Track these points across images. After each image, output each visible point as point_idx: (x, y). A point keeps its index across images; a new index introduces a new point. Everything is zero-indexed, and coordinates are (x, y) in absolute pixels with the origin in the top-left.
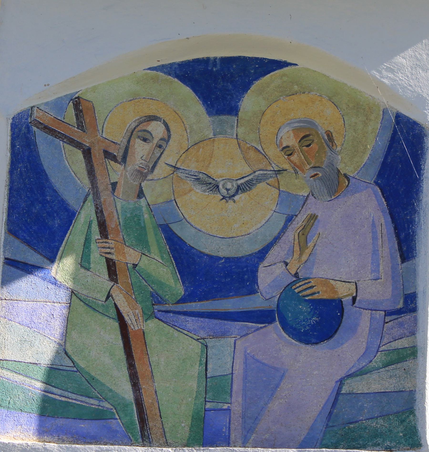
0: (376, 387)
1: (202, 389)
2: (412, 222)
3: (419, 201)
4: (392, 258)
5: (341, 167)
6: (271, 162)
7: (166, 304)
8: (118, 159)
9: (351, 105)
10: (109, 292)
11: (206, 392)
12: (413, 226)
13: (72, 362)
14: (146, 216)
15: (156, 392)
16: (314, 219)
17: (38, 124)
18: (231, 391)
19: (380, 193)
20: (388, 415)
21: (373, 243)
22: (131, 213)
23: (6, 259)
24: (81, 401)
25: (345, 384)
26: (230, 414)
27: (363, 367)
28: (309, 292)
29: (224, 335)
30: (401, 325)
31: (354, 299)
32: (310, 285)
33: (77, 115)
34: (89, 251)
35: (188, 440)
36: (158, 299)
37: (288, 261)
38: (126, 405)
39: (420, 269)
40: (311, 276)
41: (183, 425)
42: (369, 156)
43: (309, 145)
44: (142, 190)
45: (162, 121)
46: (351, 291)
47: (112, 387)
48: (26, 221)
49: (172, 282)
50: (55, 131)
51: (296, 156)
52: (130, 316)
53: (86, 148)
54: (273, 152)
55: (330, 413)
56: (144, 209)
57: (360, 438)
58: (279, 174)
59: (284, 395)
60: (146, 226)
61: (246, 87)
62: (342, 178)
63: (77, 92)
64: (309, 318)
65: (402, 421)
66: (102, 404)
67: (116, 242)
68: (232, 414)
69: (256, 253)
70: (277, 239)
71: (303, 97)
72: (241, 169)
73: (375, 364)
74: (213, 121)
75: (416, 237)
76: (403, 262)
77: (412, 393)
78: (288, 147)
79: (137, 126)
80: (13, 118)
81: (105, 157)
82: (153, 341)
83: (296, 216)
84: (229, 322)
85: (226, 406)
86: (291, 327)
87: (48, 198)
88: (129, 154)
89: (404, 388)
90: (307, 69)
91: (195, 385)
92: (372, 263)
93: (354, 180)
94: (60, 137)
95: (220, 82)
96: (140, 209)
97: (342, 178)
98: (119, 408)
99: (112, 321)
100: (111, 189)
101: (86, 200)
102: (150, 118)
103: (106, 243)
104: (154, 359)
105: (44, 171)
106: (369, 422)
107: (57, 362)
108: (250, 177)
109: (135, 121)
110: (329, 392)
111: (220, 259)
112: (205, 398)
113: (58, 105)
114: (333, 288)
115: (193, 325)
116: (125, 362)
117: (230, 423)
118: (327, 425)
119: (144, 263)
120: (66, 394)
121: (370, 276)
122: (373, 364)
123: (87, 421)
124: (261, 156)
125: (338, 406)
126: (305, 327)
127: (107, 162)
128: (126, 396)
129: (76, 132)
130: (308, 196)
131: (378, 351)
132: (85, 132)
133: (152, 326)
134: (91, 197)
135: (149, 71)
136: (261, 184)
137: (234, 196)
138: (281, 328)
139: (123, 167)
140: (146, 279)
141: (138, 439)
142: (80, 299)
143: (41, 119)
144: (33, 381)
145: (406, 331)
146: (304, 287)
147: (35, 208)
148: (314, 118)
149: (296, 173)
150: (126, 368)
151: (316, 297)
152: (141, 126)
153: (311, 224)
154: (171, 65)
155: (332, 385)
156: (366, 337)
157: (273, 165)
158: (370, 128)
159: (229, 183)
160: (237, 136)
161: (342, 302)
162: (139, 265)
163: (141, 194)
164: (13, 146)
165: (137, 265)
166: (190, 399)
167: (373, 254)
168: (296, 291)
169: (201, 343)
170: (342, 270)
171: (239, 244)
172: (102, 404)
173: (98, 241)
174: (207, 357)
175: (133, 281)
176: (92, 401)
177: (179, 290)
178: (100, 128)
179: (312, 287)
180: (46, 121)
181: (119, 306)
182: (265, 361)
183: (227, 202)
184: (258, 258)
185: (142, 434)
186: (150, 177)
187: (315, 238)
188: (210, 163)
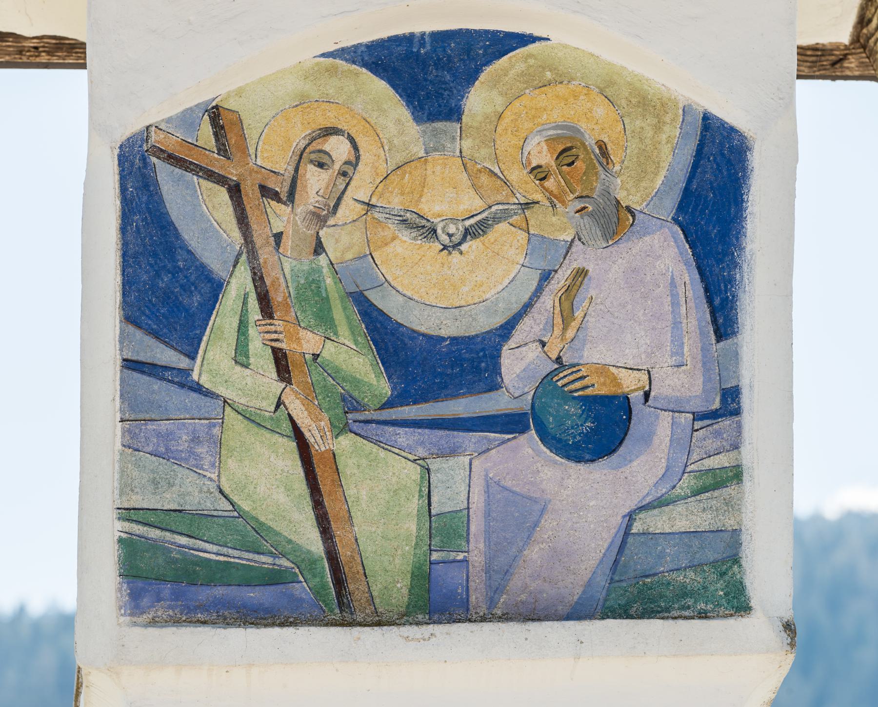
0: (682, 525)
1: (425, 532)
2: (730, 281)
3: (742, 249)
4: (703, 334)
5: (621, 195)
6: (515, 191)
7: (365, 410)
8: (282, 197)
9: (634, 101)
10: (280, 398)
11: (430, 537)
12: (732, 286)
13: (231, 504)
14: (329, 281)
15: (356, 540)
16: (583, 275)
17: (159, 152)
18: (468, 534)
19: (682, 236)
20: (701, 565)
21: (673, 312)
22: (307, 278)
23: (124, 360)
24: (248, 560)
25: (637, 520)
26: (468, 567)
27: (663, 495)
28: (578, 385)
29: (453, 452)
30: (718, 434)
31: (647, 395)
32: (580, 374)
33: (216, 134)
34: (247, 338)
35: (408, 607)
36: (352, 404)
37: (545, 339)
38: (313, 562)
39: (748, 498)
40: (581, 362)
41: (399, 585)
42: (663, 178)
43: (573, 163)
44: (321, 242)
45: (346, 135)
46: (641, 383)
47: (292, 537)
48: (150, 301)
49: (372, 378)
50: (185, 161)
51: (552, 180)
52: (313, 432)
53: (232, 184)
54: (517, 175)
55: (616, 562)
56: (325, 271)
57: (661, 598)
58: (528, 208)
59: (546, 537)
60: (330, 296)
61: (472, 77)
62: (624, 213)
63: (214, 99)
64: (579, 423)
65: (723, 574)
66: (277, 561)
67: (285, 323)
68: (470, 567)
69: (496, 329)
70: (527, 307)
71: (561, 89)
72: (470, 203)
73: (679, 491)
74: (424, 131)
75: (738, 303)
76: (718, 340)
77: (736, 533)
78: (539, 167)
79: (309, 144)
80: (121, 147)
81: (263, 196)
82: (348, 465)
83: (556, 271)
84: (461, 434)
85: (461, 556)
86: (554, 438)
87: (181, 264)
88: (298, 188)
89: (724, 525)
90: (565, 46)
91: (414, 528)
92: (672, 341)
93: (642, 215)
94: (192, 170)
95: (431, 73)
96: (319, 270)
97: (624, 213)
98: (303, 566)
99: (285, 440)
100: (273, 243)
101: (237, 263)
102: (326, 131)
103: (271, 324)
104: (350, 492)
105: (172, 224)
106: (674, 575)
107: (209, 505)
108: (484, 215)
109: (304, 138)
110: (614, 531)
111: (443, 339)
112: (430, 545)
113: (186, 119)
114: (615, 378)
115: (408, 439)
116: (308, 499)
117: (467, 581)
118: (612, 579)
119: (329, 352)
120: (225, 550)
121: (672, 361)
122: (678, 491)
123: (257, 588)
124: (499, 182)
125: (627, 551)
126: (575, 437)
127: (266, 203)
128: (313, 549)
129: (217, 160)
130: (572, 241)
131: (684, 473)
132: (229, 158)
133: (345, 443)
134: (244, 257)
135: (322, 59)
136: (500, 225)
137: (460, 244)
138: (538, 439)
139: (290, 209)
140: (333, 375)
141: (334, 609)
142: (236, 411)
143: (162, 143)
144: (175, 536)
145: (725, 444)
146: (571, 378)
147: (162, 280)
148: (578, 121)
149: (554, 206)
150: (311, 507)
151: (589, 392)
152: (314, 144)
153: (578, 283)
154: (356, 47)
155: (617, 520)
156: (666, 451)
157: (518, 195)
158: (664, 137)
159: (451, 226)
160: (461, 152)
161: (628, 399)
162: (323, 355)
163: (319, 248)
164: (123, 189)
165: (318, 355)
166: (407, 548)
167: (673, 328)
168: (560, 384)
169: (419, 465)
170: (627, 351)
171: (471, 316)
172: (277, 561)
173: (258, 323)
174: (429, 486)
175: (314, 379)
176: (263, 559)
177: (383, 388)
178: (252, 151)
179: (583, 378)
180: (170, 145)
181: (295, 418)
182: (518, 490)
183: (450, 253)
184: (500, 336)
185: (338, 601)
186: (331, 222)
187: (586, 304)
188: (421, 196)
